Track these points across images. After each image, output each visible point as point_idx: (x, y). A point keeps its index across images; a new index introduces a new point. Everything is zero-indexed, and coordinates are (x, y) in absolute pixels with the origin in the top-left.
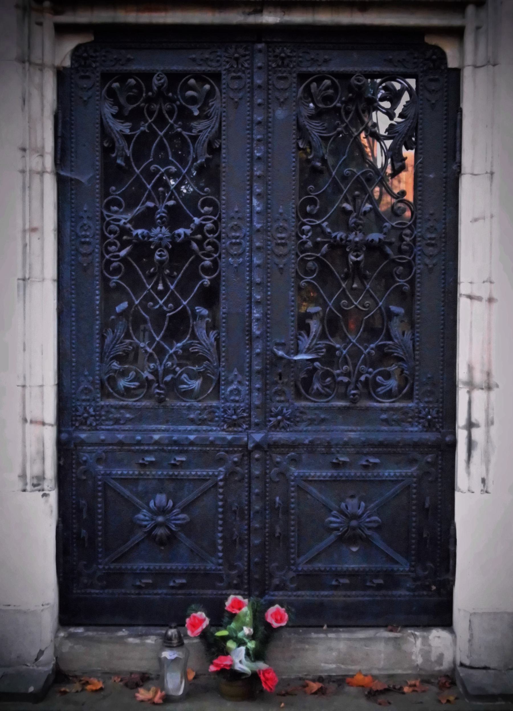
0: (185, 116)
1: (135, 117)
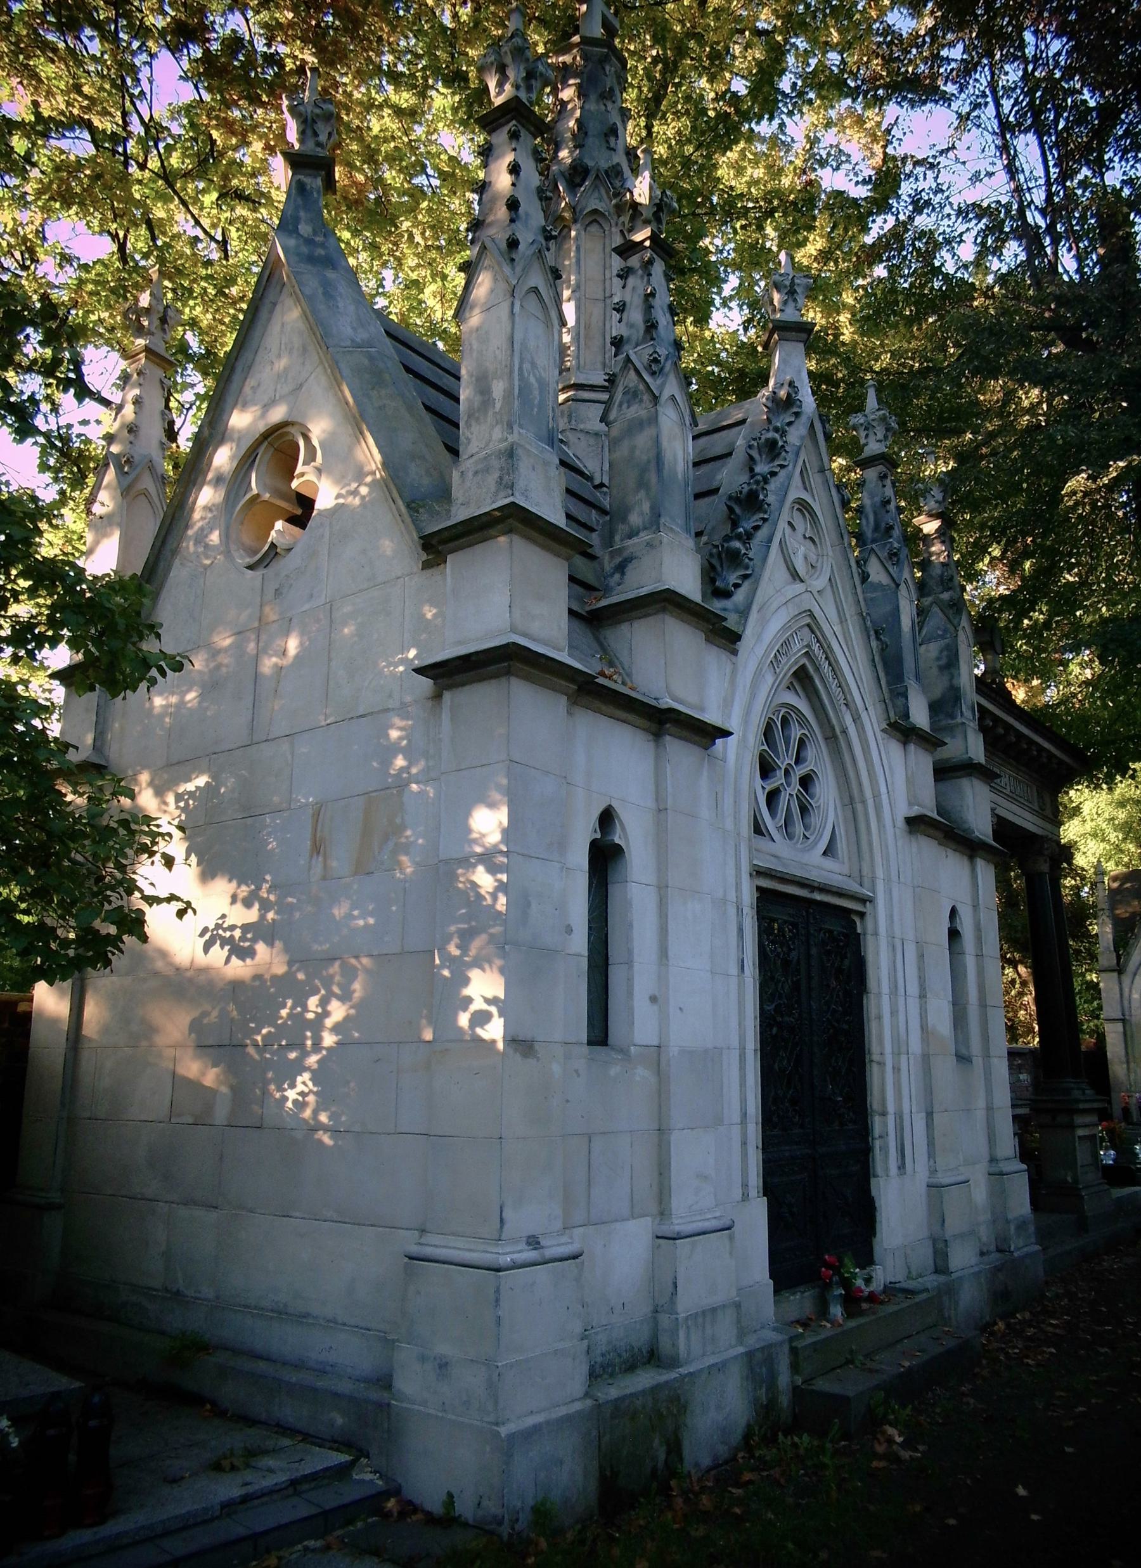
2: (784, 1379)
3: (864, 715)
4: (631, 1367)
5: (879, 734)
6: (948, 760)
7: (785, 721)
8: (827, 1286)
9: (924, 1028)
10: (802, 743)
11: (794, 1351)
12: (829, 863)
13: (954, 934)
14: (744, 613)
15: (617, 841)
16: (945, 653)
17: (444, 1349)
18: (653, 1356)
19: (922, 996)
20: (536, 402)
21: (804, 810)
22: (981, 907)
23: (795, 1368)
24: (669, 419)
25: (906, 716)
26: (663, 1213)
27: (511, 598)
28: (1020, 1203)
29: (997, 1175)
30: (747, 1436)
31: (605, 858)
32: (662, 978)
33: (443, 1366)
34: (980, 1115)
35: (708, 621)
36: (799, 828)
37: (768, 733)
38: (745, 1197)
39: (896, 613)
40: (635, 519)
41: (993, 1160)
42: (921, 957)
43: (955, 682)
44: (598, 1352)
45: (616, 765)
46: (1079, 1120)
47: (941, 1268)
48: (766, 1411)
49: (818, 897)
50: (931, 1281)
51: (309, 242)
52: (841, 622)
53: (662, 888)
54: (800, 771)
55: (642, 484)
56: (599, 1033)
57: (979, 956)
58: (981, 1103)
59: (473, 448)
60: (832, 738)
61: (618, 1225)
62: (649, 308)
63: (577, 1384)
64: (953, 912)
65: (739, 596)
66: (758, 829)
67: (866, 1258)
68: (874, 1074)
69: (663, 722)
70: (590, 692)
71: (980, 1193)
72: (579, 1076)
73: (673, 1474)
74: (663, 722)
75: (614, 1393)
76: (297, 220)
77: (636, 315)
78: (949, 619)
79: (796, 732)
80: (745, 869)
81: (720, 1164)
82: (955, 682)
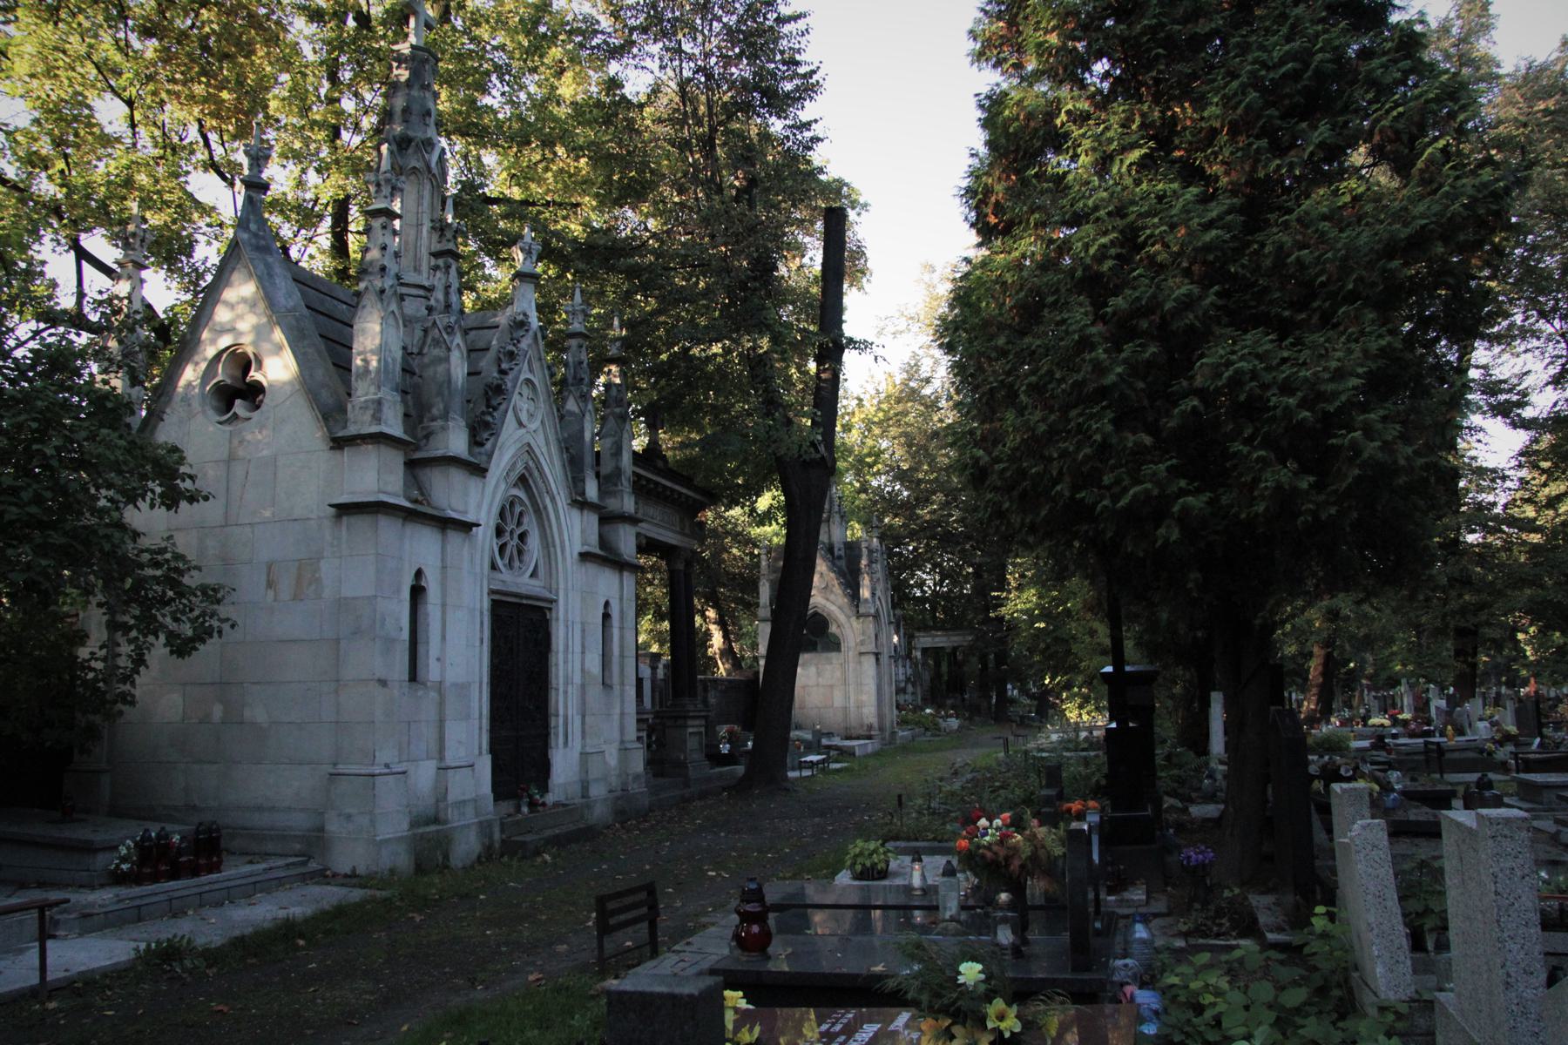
2: (497, 836)
4: (427, 824)
7: (512, 504)
8: (521, 798)
9: (583, 670)
10: (521, 514)
11: (502, 824)
12: (533, 582)
13: (606, 616)
14: (490, 456)
17: (348, 810)
19: (583, 653)
21: (520, 552)
23: (502, 831)
24: (456, 357)
25: (583, 493)
26: (442, 758)
27: (374, 476)
28: (638, 763)
29: (624, 750)
30: (479, 857)
31: (417, 592)
32: (443, 650)
33: (349, 817)
34: (616, 717)
36: (517, 564)
37: (502, 515)
39: (582, 431)
40: (435, 411)
41: (622, 742)
42: (583, 631)
45: (423, 547)
46: (690, 722)
47: (585, 795)
48: (488, 849)
50: (578, 801)
51: (256, 235)
53: (444, 605)
54: (519, 532)
55: (440, 393)
56: (413, 676)
57: (622, 628)
58: (617, 711)
59: (359, 393)
60: (539, 512)
62: (447, 294)
63: (405, 826)
64: (607, 604)
65: (488, 445)
66: (494, 567)
67: (544, 789)
68: (553, 694)
69: (445, 524)
70: (411, 515)
71: (612, 759)
73: (447, 867)
74: (445, 524)
75: (421, 830)
76: (248, 221)
77: (439, 295)
79: (518, 509)
80: (486, 591)
81: (469, 736)
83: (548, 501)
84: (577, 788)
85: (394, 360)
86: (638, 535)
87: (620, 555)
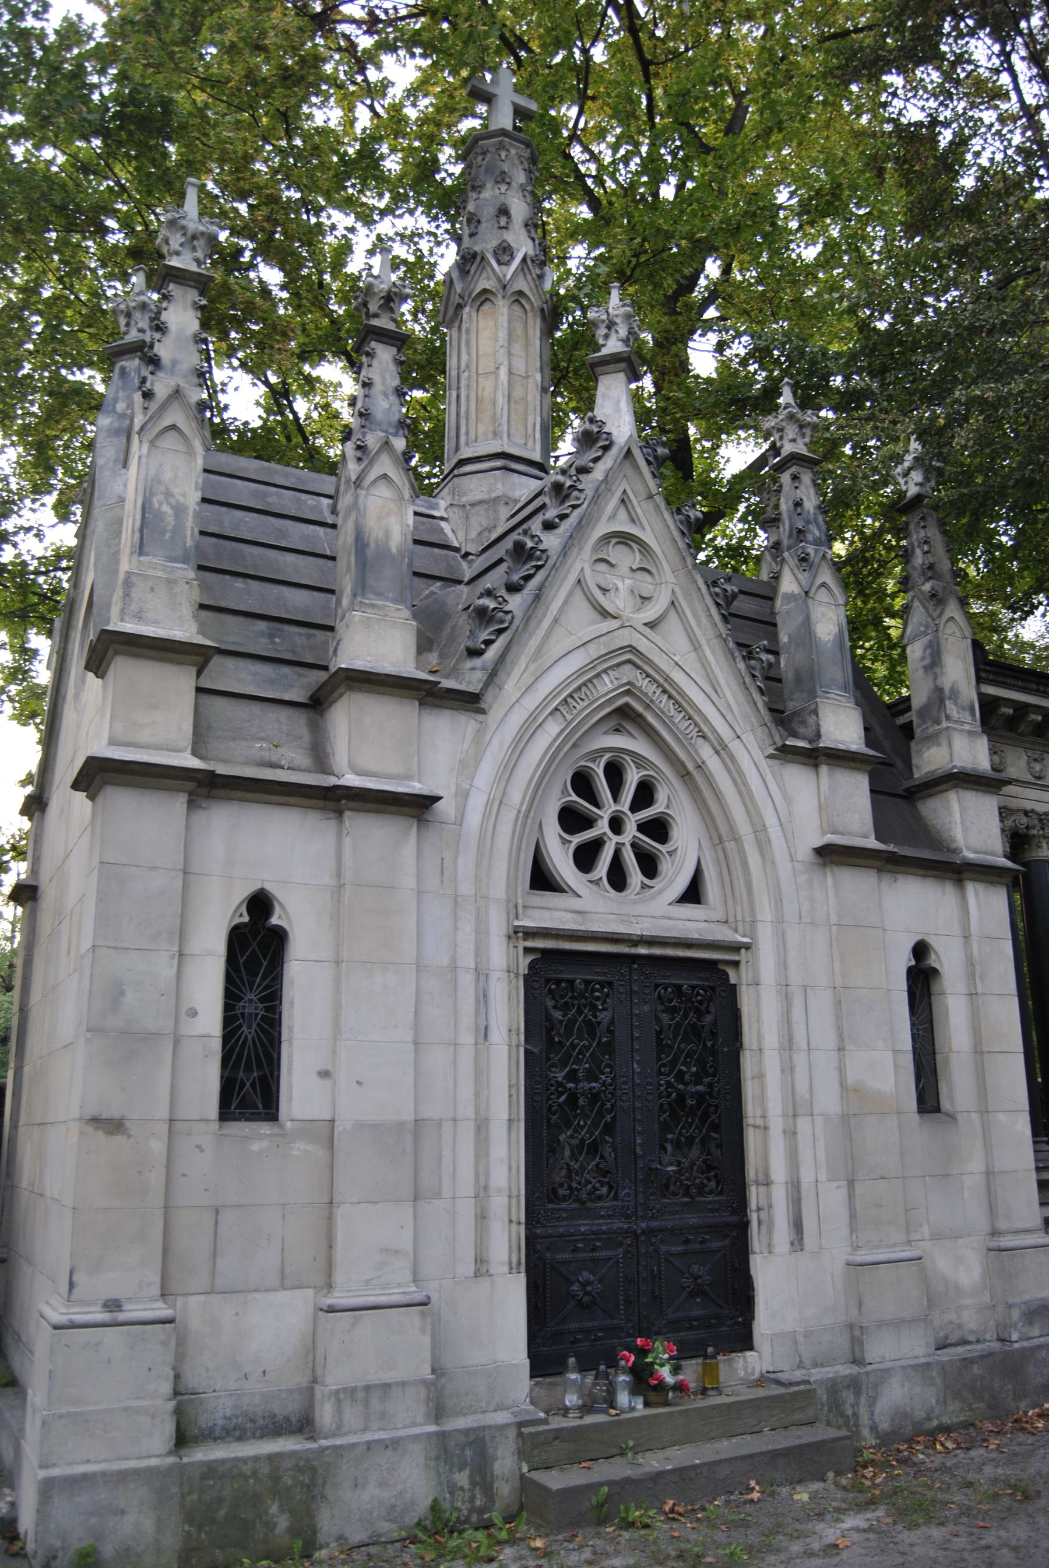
0: (594, 1008)
1: (565, 1008)
3: (735, 746)
5: (764, 764)
6: (931, 772)
12: (689, 910)
15: (934, 965)
16: (928, 651)
18: (303, 1425)
20: (170, 527)
22: (974, 938)
35: (418, 689)
38: (481, 1266)
43: (938, 682)
44: (220, 1414)
49: (643, 951)
52: (695, 649)
58: (976, 1165)
61: (258, 1295)
66: (542, 879)
68: (752, 1139)
72: (202, 1151)
78: (927, 611)
79: (632, 778)
82: (938, 682)
83: (706, 752)
84: (843, 1345)
85: (179, 510)
86: (1004, 812)
87: (955, 851)
